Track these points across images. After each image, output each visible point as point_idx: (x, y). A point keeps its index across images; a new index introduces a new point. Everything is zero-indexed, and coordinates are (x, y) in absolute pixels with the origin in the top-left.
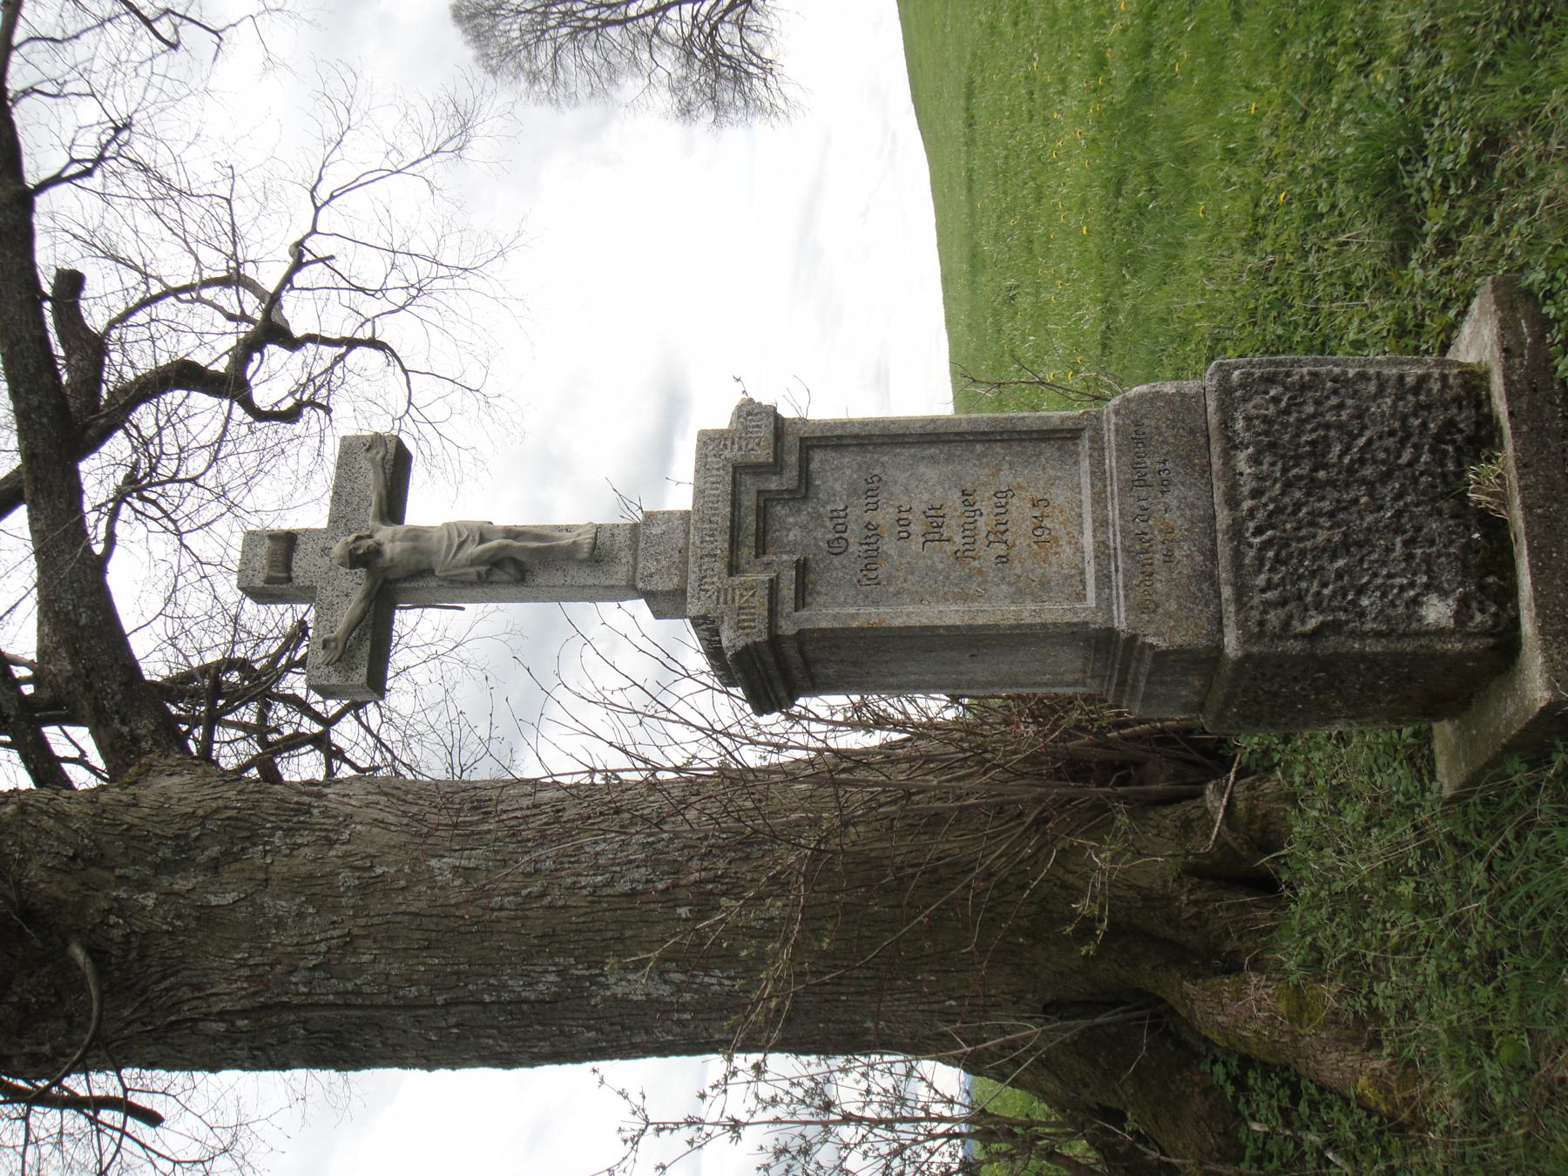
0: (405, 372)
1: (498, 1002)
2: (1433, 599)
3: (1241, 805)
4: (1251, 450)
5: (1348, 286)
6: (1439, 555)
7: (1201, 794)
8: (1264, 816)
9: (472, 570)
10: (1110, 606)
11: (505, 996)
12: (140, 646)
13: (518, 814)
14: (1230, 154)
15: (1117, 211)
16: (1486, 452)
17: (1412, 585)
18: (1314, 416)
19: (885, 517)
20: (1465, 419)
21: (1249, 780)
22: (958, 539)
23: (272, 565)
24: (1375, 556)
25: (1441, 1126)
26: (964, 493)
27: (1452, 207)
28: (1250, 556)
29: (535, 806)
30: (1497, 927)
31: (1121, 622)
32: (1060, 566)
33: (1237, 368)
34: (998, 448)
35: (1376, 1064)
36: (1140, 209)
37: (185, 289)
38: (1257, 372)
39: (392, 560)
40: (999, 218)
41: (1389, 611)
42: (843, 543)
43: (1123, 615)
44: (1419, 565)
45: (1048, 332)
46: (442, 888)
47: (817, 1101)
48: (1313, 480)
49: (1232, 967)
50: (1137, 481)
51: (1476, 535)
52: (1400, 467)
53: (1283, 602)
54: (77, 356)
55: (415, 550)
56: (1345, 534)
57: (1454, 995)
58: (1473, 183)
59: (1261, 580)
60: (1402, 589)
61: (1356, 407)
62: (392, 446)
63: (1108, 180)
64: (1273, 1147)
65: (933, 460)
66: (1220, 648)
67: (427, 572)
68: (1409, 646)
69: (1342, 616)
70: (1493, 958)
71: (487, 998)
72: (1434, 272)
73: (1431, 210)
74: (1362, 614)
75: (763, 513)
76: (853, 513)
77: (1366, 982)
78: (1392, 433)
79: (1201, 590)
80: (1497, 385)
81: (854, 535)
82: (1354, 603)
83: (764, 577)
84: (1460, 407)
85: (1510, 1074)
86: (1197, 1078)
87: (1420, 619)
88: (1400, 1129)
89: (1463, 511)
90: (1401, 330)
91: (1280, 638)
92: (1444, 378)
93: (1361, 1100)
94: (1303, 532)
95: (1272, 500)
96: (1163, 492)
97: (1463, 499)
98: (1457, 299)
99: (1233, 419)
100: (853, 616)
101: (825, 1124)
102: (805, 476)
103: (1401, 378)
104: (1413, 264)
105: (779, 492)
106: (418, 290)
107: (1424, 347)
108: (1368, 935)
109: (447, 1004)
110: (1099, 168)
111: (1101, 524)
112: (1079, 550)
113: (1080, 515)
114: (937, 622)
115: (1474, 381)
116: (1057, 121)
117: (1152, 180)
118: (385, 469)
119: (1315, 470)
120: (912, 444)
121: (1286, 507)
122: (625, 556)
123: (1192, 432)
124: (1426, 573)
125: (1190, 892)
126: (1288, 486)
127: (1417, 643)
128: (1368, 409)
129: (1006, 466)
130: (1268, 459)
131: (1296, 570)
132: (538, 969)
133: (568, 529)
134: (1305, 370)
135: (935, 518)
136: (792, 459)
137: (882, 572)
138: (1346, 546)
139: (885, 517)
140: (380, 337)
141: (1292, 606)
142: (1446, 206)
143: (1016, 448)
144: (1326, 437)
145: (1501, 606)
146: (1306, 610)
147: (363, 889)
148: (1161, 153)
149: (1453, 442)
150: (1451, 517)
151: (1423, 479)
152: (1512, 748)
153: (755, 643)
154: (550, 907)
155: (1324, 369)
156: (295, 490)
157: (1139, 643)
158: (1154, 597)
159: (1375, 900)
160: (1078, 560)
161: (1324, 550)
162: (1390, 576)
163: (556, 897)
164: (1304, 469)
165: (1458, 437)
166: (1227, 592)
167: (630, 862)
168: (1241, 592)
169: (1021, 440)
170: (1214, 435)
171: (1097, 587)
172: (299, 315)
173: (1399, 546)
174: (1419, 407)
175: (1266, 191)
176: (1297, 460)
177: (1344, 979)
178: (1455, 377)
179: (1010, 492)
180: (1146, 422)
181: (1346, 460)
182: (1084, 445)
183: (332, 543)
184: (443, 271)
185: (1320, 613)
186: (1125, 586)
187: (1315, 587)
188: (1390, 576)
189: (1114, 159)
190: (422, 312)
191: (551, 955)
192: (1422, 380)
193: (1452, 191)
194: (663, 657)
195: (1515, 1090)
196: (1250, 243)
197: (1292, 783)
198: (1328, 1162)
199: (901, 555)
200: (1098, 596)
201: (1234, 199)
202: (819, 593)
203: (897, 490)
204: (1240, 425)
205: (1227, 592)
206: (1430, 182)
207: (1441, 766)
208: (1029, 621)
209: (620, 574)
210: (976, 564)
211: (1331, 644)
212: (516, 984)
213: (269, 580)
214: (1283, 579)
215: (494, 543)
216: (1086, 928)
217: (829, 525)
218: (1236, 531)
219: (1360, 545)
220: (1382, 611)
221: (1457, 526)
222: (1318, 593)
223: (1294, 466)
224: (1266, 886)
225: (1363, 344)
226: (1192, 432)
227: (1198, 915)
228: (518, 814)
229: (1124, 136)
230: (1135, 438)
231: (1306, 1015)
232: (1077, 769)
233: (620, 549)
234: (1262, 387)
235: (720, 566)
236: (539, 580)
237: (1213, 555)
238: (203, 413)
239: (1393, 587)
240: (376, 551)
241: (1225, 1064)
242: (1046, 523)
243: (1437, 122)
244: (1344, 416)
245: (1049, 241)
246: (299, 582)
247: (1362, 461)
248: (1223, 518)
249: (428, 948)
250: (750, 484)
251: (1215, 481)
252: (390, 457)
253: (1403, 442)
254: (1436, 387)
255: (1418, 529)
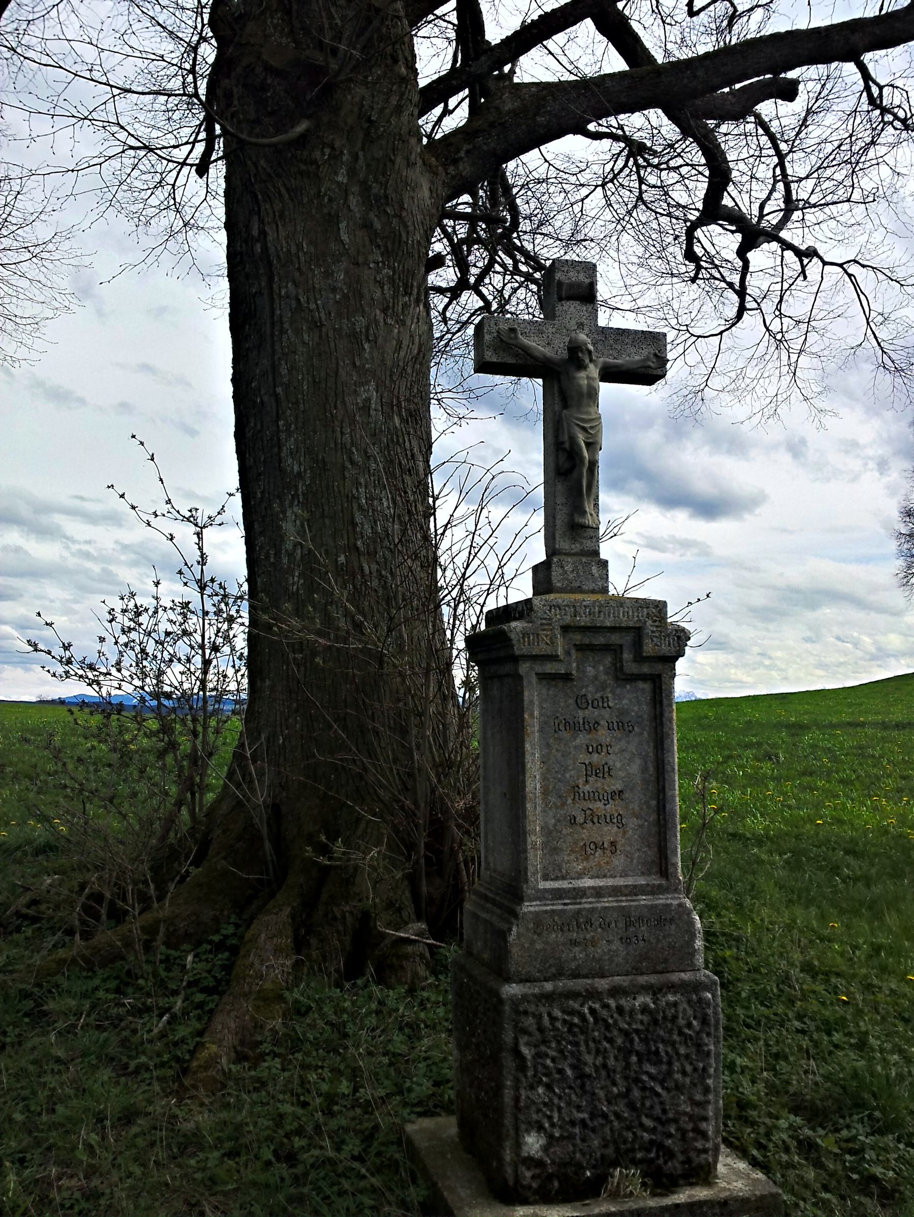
0: (721, 333)
1: (278, 431)
2: (542, 1141)
3: (410, 949)
4: (652, 1006)
5: (777, 1056)
6: (574, 1145)
7: (419, 919)
8: (402, 967)
9: (566, 437)
10: (540, 899)
11: (283, 436)
12: (532, 158)
13: (407, 444)
14: (877, 949)
15: (834, 849)
16: (649, 1181)
17: (553, 1125)
18: (677, 1054)
19: (604, 736)
20: (674, 1166)
21: (428, 955)
22: (587, 788)
23: (571, 285)
24: (574, 1097)
25: (178, 1112)
26: (621, 792)
27: (836, 1155)
28: (574, 1004)
29: (413, 456)
30: (312, 1166)
31: (529, 907)
32: (568, 862)
33: (713, 996)
34: (653, 817)
35: (224, 1060)
36: (835, 870)
37: (783, 169)
38: (710, 1011)
39: (574, 378)
40: (829, 749)
41: (534, 1108)
42: (585, 706)
43: (532, 909)
44: (567, 1131)
45: (745, 787)
46: (355, 391)
47: (220, 640)
48: (630, 1052)
49: (299, 945)
50: (629, 918)
51: (588, 1174)
52: (639, 1117)
53: (541, 1029)
54: (734, 100)
55: (581, 395)
56: (590, 1076)
57: (268, 1128)
58: (855, 1176)
59: (557, 1013)
60: (550, 1118)
61: (684, 1085)
62: (659, 372)
63: (857, 844)
64: (176, 972)
65: (644, 770)
66: (508, 980)
67: (565, 404)
68: (508, 1121)
69: (530, 1073)
70: (291, 1158)
71: (281, 423)
72: (784, 1136)
73: (832, 1138)
74: (532, 1087)
75: (606, 648)
76: (606, 714)
77: (282, 1050)
78: (664, 1111)
79: (551, 966)
80: (702, 1193)
81: (590, 713)
82: (540, 1082)
83: (560, 651)
84: (683, 1163)
85: (208, 1173)
86: (226, 913)
87: (528, 1132)
88: (177, 1078)
89: (606, 1164)
90: (743, 1105)
91: (515, 1026)
92: (705, 1151)
93: (199, 1046)
94: (592, 1045)
95: (616, 1022)
96: (621, 939)
97: (615, 1164)
98: (765, 1156)
99: (675, 993)
100: (532, 715)
101: (202, 647)
102: (633, 678)
103: (705, 1119)
104: (792, 1117)
105: (621, 661)
106: (780, 341)
107: (730, 1123)
108: (314, 1054)
109: (276, 395)
110: (866, 836)
111: (598, 893)
112: (580, 876)
113: (605, 876)
114: (528, 775)
115: (703, 1174)
116: (901, 800)
117: (856, 880)
118: (642, 361)
119: (638, 1054)
120: (656, 755)
121: (610, 1031)
122: (576, 547)
123: (666, 961)
124: (561, 1136)
125: (351, 913)
126: (626, 1034)
127: (510, 1127)
128: (682, 1094)
129: (640, 822)
130: (645, 1018)
131: (564, 1039)
132: (302, 459)
133: (596, 505)
134: (712, 1047)
135: (602, 772)
136: (646, 669)
137: (565, 735)
138: (582, 1076)
139: (604, 736)
140: (745, 315)
141: (538, 1035)
142: (837, 1151)
143: (654, 830)
144: (661, 1062)
145: (536, 1192)
146: (536, 1046)
147: (354, 336)
148: (877, 890)
149: (658, 1157)
150: (602, 1155)
151: (630, 1135)
152: (433, 1187)
153: (512, 646)
154: (344, 468)
155: (712, 1061)
156: (629, 294)
157: (513, 920)
158: (545, 932)
159: (338, 1059)
160: (573, 874)
161: (579, 1060)
162: (559, 1109)
163: (351, 472)
164: (638, 1045)
165: (661, 1161)
166: (549, 986)
167: (375, 522)
168: (548, 998)
169: (659, 833)
170: (662, 978)
171: (553, 889)
172: (763, 257)
173: (581, 1116)
174: (684, 1132)
175: (848, 983)
176: (645, 1041)
177: (285, 1035)
178: (706, 1160)
179: (621, 825)
180: (673, 927)
181: (645, 1078)
182: (656, 880)
183: (587, 331)
184: (794, 357)
185: (533, 1057)
186: (553, 911)
187: (552, 1053)
188: (559, 1109)
189: (873, 849)
190: (764, 344)
191: (311, 468)
192: (704, 1135)
193: (848, 1157)
194: (512, 551)
195: (198, 1176)
196: (807, 968)
197: (423, 989)
198: (161, 1016)
199: (575, 747)
200: (546, 890)
201: (842, 954)
202: (549, 689)
203: (623, 744)
204: (671, 998)
205: (549, 986)
206: (853, 1139)
207: (426, 1123)
208: (529, 840)
209: (563, 544)
210: (570, 801)
211: (509, 1063)
212: (291, 444)
213: (560, 283)
214: (558, 1029)
215: (586, 454)
216: (324, 850)
217: (598, 695)
218: (593, 994)
219: (582, 1086)
220: (534, 1103)
221: (596, 1160)
222: (547, 1055)
223: (641, 1040)
224: (353, 971)
225: (731, 1072)
226: (666, 961)
227: (335, 918)
228: (407, 444)
229: (890, 857)
230: (663, 918)
231: (261, 1003)
232: (438, 830)
233: (581, 544)
234: (699, 1015)
235: (568, 619)
236: (559, 487)
237: (575, 975)
238: (693, 192)
239: (552, 1111)
240: (582, 366)
241: (234, 934)
242: (599, 852)
243: (901, 1146)
244: (678, 1076)
245: (812, 790)
246: (559, 308)
247: (644, 1089)
248: (602, 984)
249: (314, 381)
250: (626, 640)
251: (630, 977)
252: (650, 372)
253: (658, 1119)
254: (699, 1145)
255: (593, 1130)
